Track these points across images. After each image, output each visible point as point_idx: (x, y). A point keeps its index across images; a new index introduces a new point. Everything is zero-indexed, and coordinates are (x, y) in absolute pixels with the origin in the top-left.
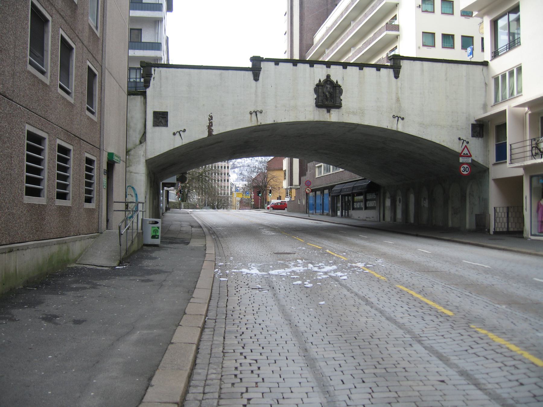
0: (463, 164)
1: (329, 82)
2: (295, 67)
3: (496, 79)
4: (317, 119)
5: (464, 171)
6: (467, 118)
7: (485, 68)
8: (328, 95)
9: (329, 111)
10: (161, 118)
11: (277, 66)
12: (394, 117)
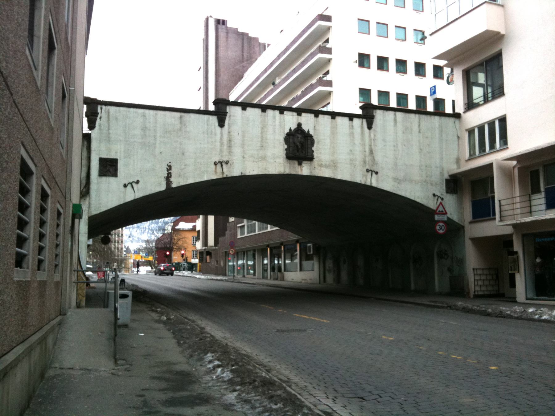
0: (439, 221)
1: (299, 132)
2: (264, 114)
3: (471, 132)
4: (287, 171)
5: (440, 229)
6: (441, 173)
7: (457, 121)
8: (299, 145)
9: (300, 164)
10: (109, 167)
11: (244, 111)
12: (368, 171)
